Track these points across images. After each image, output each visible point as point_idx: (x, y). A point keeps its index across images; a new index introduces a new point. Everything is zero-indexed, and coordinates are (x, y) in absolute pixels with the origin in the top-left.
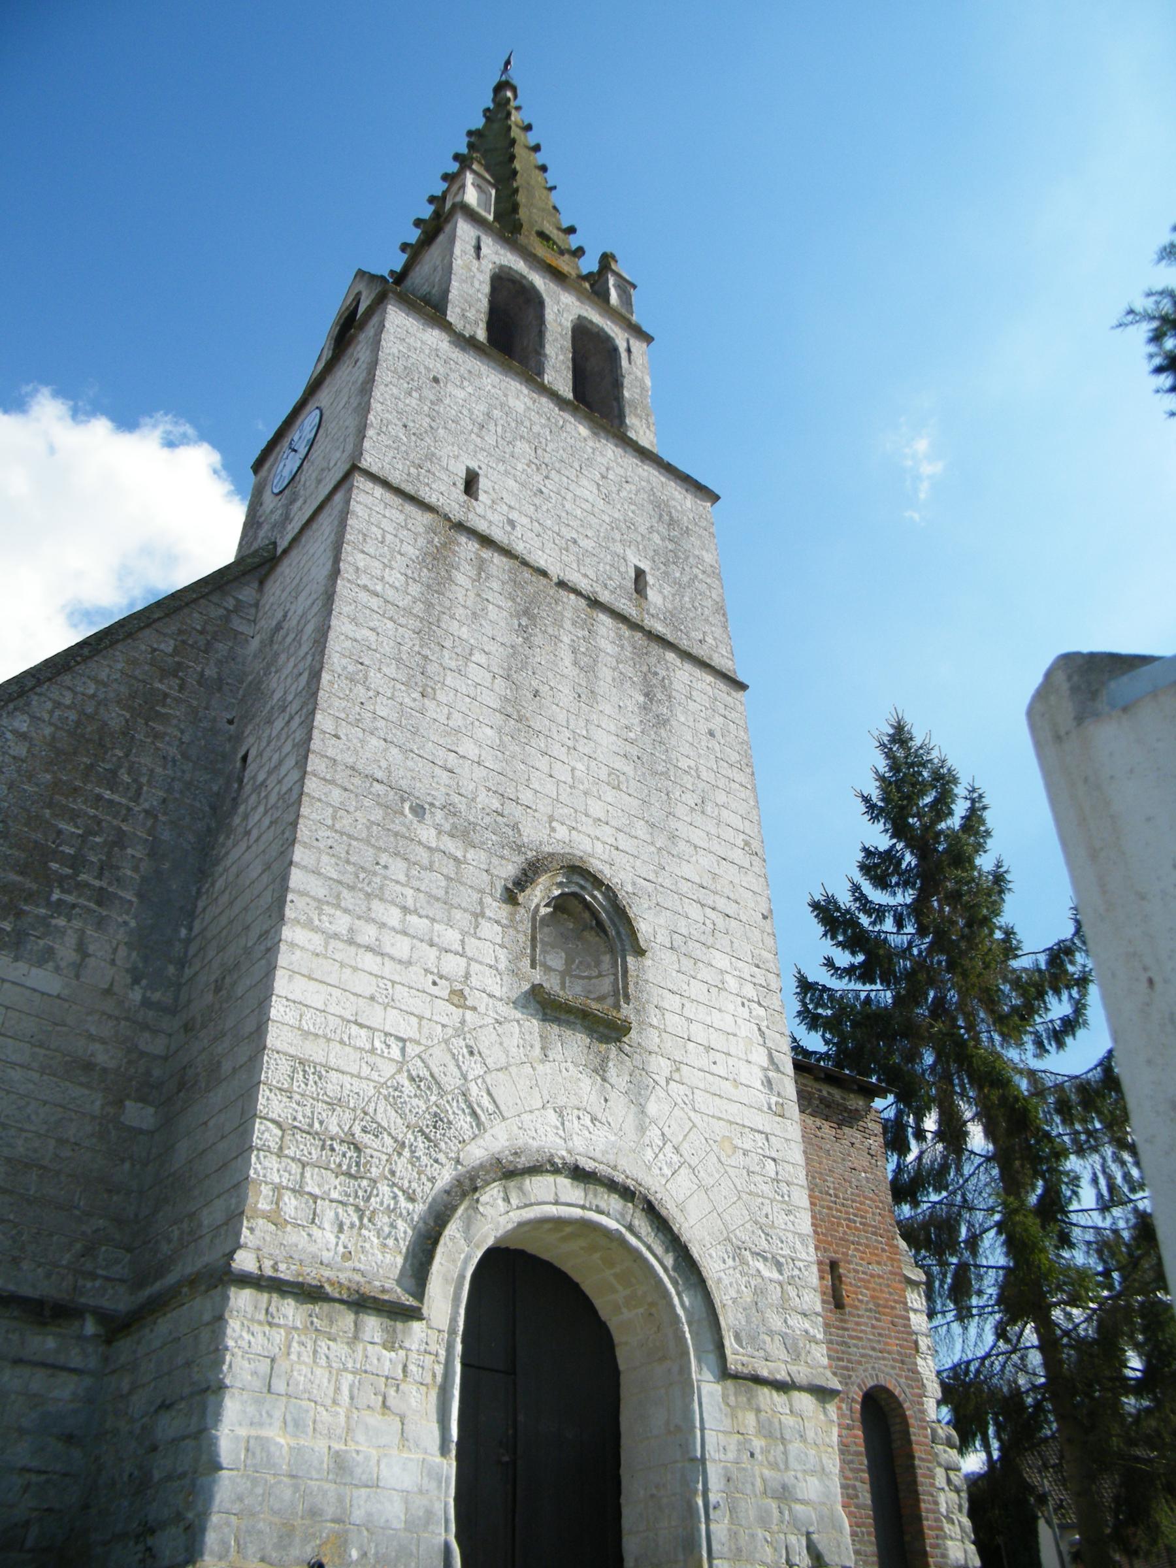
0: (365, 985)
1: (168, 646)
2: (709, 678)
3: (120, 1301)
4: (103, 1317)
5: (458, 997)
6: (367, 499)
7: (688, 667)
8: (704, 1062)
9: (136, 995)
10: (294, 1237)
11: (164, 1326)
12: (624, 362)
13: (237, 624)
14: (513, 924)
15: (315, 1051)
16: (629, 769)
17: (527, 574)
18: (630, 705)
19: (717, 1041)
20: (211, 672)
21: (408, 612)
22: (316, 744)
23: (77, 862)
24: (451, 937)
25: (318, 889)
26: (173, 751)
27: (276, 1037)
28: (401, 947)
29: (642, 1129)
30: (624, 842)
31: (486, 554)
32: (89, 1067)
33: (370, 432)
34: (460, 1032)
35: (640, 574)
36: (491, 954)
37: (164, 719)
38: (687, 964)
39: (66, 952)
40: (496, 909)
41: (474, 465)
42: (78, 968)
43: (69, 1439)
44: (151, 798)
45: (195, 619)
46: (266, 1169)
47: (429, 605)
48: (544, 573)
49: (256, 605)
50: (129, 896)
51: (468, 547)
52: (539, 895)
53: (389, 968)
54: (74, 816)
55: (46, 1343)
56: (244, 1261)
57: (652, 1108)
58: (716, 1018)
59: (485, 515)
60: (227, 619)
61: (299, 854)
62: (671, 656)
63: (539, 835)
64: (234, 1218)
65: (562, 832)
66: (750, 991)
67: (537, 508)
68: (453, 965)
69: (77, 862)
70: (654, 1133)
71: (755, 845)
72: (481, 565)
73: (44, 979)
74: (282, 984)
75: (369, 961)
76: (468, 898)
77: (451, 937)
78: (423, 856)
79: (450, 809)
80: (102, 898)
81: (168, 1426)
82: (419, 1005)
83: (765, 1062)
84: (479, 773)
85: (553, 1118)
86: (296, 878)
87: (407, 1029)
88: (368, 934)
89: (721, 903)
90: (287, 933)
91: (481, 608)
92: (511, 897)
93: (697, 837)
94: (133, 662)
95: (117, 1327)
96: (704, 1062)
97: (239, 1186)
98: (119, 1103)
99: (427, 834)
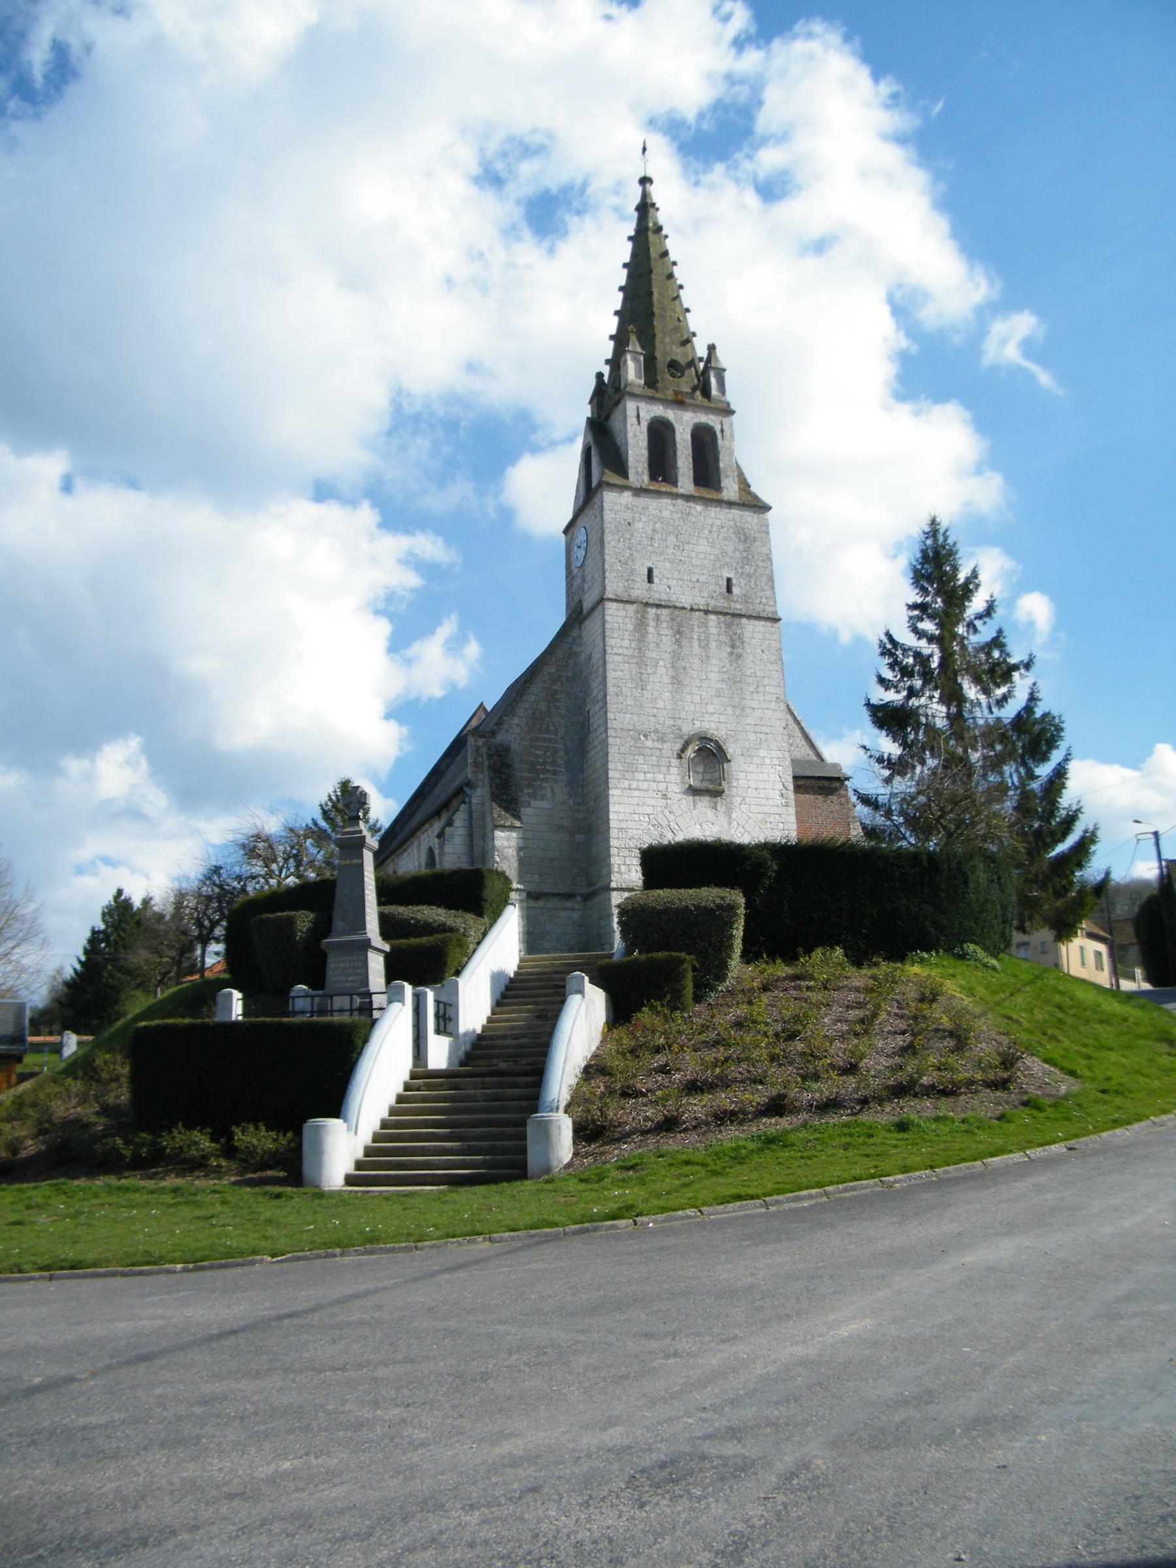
0: (635, 801)
1: (553, 670)
2: (763, 623)
3: (585, 891)
4: (582, 895)
5: (665, 797)
6: (611, 609)
7: (752, 622)
8: (755, 794)
9: (571, 801)
10: (626, 876)
11: (597, 900)
12: (720, 442)
13: (576, 649)
14: (681, 765)
15: (624, 825)
16: (724, 686)
17: (677, 612)
18: (724, 655)
19: (760, 785)
20: (570, 674)
21: (632, 656)
22: (609, 725)
23: (544, 763)
24: (660, 777)
25: (617, 775)
26: (564, 712)
27: (613, 824)
28: (645, 785)
29: (730, 823)
30: (722, 719)
31: (660, 611)
32: (563, 827)
33: (607, 574)
34: (666, 807)
35: (729, 580)
36: (674, 778)
37: (558, 700)
38: (749, 759)
39: (548, 793)
40: (675, 762)
41: (650, 565)
42: (553, 798)
43: (580, 926)
44: (561, 733)
45: (560, 653)
46: (615, 860)
47: (640, 649)
48: (684, 608)
49: (580, 636)
50: (562, 769)
51: (652, 611)
52: (690, 753)
53: (642, 794)
54: (539, 748)
55: (568, 904)
56: (613, 885)
57: (734, 816)
58: (760, 777)
59: (659, 591)
60: (571, 648)
61: (610, 766)
62: (744, 620)
63: (688, 729)
64: (609, 873)
65: (697, 724)
66: (776, 762)
67: (679, 571)
68: (662, 786)
69: (544, 763)
70: (735, 824)
71: (782, 697)
72: (658, 618)
73: (545, 804)
74: (611, 808)
75: (636, 793)
76: (665, 761)
77: (660, 777)
78: (649, 751)
79: (656, 731)
80: (555, 773)
81: (602, 923)
82: (652, 802)
83: (781, 787)
84: (665, 712)
85: (698, 826)
86: (611, 774)
87: (650, 811)
88: (634, 784)
89: (765, 729)
90: (611, 792)
91: (660, 633)
92: (680, 757)
93: (754, 704)
94: (544, 682)
95: (587, 898)
96: (755, 794)
97: (609, 865)
98: (573, 836)
99: (649, 744)
